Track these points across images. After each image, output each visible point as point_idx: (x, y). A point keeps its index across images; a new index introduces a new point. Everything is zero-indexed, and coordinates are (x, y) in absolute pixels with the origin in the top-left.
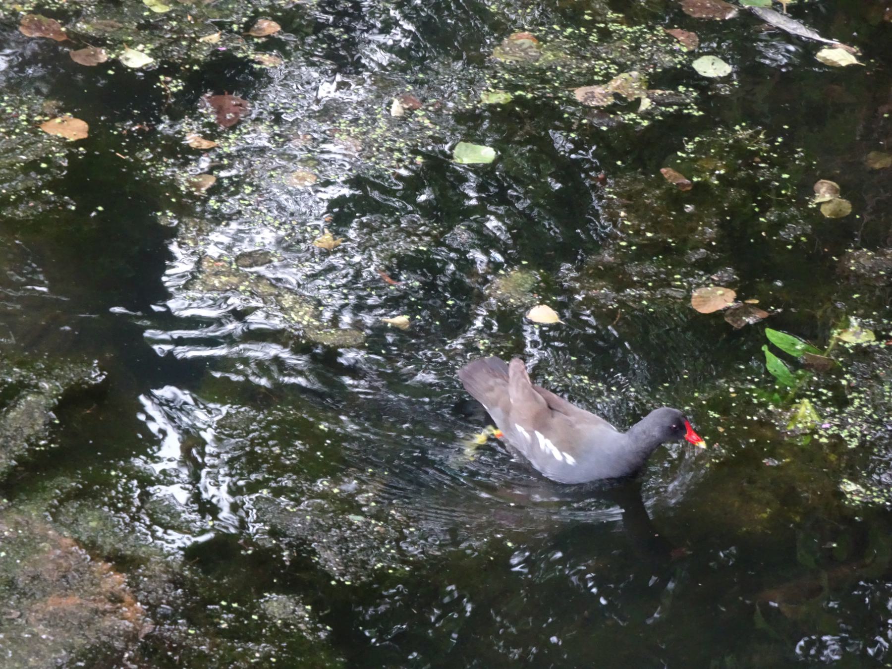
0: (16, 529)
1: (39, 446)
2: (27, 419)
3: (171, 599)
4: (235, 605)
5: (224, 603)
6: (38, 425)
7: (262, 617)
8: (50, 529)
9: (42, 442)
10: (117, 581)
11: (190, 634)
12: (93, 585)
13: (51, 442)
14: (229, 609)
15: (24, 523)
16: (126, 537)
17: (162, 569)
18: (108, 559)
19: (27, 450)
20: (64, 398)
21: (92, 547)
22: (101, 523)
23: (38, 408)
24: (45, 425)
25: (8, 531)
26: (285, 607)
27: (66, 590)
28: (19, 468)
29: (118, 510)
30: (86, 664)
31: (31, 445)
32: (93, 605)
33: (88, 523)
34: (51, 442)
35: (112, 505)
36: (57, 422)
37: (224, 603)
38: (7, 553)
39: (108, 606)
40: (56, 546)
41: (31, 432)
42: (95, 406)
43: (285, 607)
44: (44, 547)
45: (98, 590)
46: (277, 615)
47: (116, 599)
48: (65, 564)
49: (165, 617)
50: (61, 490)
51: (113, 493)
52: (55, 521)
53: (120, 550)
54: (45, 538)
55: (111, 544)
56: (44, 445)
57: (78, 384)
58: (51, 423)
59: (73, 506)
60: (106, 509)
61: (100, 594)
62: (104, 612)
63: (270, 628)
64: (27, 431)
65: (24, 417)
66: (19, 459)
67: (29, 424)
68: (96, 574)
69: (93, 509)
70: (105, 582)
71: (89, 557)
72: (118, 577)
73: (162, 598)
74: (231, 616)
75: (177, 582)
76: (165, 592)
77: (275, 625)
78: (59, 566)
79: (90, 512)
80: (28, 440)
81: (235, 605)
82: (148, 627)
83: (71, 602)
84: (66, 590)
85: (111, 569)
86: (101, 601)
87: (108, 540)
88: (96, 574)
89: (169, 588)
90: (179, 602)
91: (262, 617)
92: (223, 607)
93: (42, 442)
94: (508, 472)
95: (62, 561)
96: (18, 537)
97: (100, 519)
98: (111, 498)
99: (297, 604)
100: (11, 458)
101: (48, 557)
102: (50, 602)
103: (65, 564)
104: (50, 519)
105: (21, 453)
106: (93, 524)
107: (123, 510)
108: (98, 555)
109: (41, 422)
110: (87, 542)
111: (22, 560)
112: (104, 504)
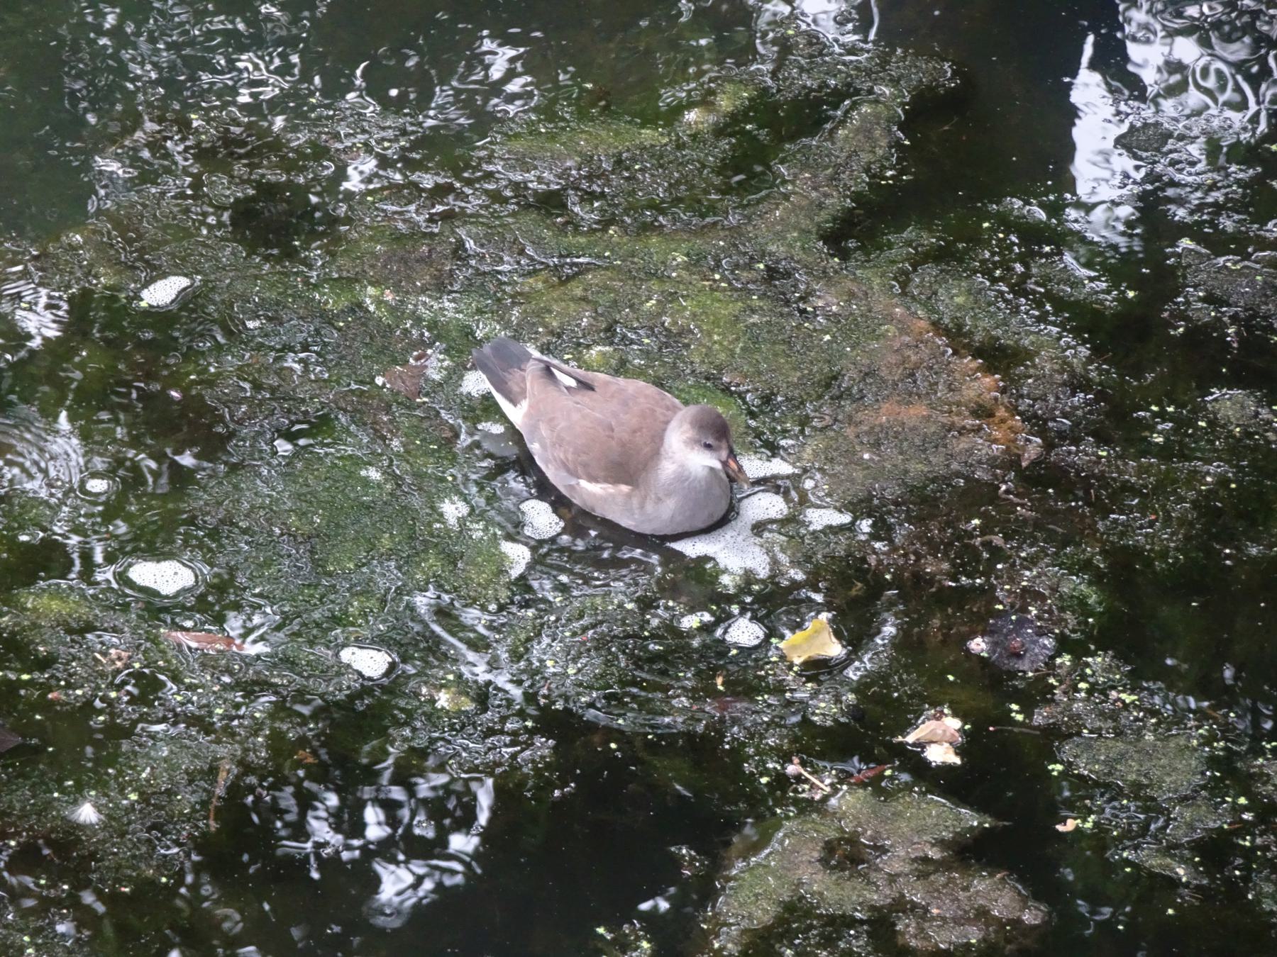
0: (848, 301)
1: (886, 179)
2: (863, 140)
3: (1068, 409)
4: (1171, 409)
5: (1154, 408)
6: (881, 147)
7: (1212, 423)
8: (897, 306)
9: (889, 173)
10: (985, 385)
11: (1102, 457)
12: (951, 390)
13: (902, 172)
14: (1163, 415)
15: (860, 295)
16: (1005, 323)
17: (1056, 367)
18: (977, 353)
19: (867, 184)
20: (912, 109)
21: (956, 335)
22: (972, 298)
23: (878, 124)
24: (890, 147)
25: (838, 304)
26: (1243, 407)
27: (910, 394)
28: (858, 211)
29: (994, 281)
30: (132, 891)
31: (872, 177)
32: (944, 419)
33: (952, 298)
34: (902, 172)
35: (988, 273)
36: (907, 143)
37: (1154, 408)
38: (833, 336)
39: (970, 422)
40: (903, 331)
41: (871, 157)
42: (956, 119)
43: (1243, 407)
44: (887, 331)
45: (957, 398)
46: (1233, 420)
47: (983, 412)
48: (913, 358)
49: (1062, 435)
50: (915, 249)
51: (987, 254)
52: (904, 294)
53: (998, 339)
54: (890, 318)
55: (985, 329)
56: (892, 177)
57: (930, 88)
58: (898, 144)
59: (931, 270)
60: (980, 279)
61: (958, 404)
62: (962, 431)
63: (1226, 438)
64: (865, 157)
65: (860, 137)
66: (857, 197)
67: (867, 147)
68: (957, 376)
69: (960, 278)
70: (969, 388)
71: (950, 351)
72: (988, 380)
73: (1055, 409)
74: (1169, 425)
75: (1078, 383)
76: (1058, 398)
77: (1230, 434)
78: (905, 360)
79: (956, 282)
80: (867, 170)
81: (1171, 409)
82: (1033, 448)
83: (916, 412)
84: (910, 394)
85: (978, 369)
86: (959, 414)
87: (980, 323)
88: (957, 376)
89: (1064, 394)
90: (1079, 413)
91: (1212, 423)
92: (1155, 415)
93: (889, 173)
94: (487, 338)
95: (910, 353)
96: (851, 314)
97: (969, 292)
98: (983, 262)
99: (1259, 403)
100: (845, 197)
101: (892, 346)
102: (883, 411)
103: (913, 358)
104: (897, 290)
105: (859, 188)
106: (959, 300)
107: (1001, 279)
108: (965, 346)
109: (884, 143)
110: (950, 325)
111: (853, 348)
112: (975, 272)
